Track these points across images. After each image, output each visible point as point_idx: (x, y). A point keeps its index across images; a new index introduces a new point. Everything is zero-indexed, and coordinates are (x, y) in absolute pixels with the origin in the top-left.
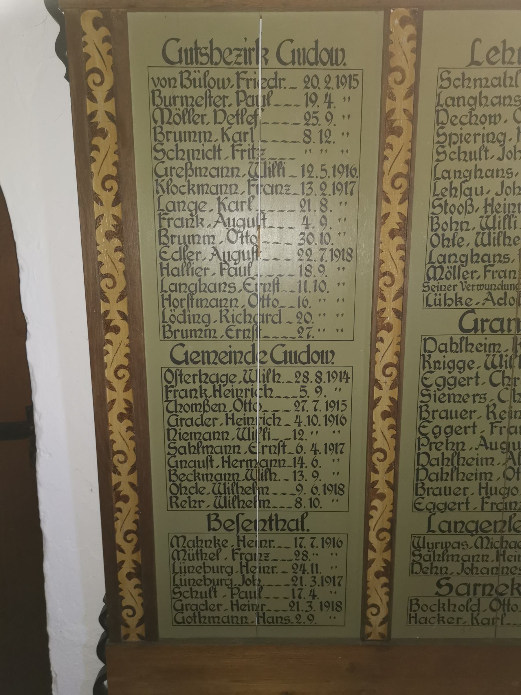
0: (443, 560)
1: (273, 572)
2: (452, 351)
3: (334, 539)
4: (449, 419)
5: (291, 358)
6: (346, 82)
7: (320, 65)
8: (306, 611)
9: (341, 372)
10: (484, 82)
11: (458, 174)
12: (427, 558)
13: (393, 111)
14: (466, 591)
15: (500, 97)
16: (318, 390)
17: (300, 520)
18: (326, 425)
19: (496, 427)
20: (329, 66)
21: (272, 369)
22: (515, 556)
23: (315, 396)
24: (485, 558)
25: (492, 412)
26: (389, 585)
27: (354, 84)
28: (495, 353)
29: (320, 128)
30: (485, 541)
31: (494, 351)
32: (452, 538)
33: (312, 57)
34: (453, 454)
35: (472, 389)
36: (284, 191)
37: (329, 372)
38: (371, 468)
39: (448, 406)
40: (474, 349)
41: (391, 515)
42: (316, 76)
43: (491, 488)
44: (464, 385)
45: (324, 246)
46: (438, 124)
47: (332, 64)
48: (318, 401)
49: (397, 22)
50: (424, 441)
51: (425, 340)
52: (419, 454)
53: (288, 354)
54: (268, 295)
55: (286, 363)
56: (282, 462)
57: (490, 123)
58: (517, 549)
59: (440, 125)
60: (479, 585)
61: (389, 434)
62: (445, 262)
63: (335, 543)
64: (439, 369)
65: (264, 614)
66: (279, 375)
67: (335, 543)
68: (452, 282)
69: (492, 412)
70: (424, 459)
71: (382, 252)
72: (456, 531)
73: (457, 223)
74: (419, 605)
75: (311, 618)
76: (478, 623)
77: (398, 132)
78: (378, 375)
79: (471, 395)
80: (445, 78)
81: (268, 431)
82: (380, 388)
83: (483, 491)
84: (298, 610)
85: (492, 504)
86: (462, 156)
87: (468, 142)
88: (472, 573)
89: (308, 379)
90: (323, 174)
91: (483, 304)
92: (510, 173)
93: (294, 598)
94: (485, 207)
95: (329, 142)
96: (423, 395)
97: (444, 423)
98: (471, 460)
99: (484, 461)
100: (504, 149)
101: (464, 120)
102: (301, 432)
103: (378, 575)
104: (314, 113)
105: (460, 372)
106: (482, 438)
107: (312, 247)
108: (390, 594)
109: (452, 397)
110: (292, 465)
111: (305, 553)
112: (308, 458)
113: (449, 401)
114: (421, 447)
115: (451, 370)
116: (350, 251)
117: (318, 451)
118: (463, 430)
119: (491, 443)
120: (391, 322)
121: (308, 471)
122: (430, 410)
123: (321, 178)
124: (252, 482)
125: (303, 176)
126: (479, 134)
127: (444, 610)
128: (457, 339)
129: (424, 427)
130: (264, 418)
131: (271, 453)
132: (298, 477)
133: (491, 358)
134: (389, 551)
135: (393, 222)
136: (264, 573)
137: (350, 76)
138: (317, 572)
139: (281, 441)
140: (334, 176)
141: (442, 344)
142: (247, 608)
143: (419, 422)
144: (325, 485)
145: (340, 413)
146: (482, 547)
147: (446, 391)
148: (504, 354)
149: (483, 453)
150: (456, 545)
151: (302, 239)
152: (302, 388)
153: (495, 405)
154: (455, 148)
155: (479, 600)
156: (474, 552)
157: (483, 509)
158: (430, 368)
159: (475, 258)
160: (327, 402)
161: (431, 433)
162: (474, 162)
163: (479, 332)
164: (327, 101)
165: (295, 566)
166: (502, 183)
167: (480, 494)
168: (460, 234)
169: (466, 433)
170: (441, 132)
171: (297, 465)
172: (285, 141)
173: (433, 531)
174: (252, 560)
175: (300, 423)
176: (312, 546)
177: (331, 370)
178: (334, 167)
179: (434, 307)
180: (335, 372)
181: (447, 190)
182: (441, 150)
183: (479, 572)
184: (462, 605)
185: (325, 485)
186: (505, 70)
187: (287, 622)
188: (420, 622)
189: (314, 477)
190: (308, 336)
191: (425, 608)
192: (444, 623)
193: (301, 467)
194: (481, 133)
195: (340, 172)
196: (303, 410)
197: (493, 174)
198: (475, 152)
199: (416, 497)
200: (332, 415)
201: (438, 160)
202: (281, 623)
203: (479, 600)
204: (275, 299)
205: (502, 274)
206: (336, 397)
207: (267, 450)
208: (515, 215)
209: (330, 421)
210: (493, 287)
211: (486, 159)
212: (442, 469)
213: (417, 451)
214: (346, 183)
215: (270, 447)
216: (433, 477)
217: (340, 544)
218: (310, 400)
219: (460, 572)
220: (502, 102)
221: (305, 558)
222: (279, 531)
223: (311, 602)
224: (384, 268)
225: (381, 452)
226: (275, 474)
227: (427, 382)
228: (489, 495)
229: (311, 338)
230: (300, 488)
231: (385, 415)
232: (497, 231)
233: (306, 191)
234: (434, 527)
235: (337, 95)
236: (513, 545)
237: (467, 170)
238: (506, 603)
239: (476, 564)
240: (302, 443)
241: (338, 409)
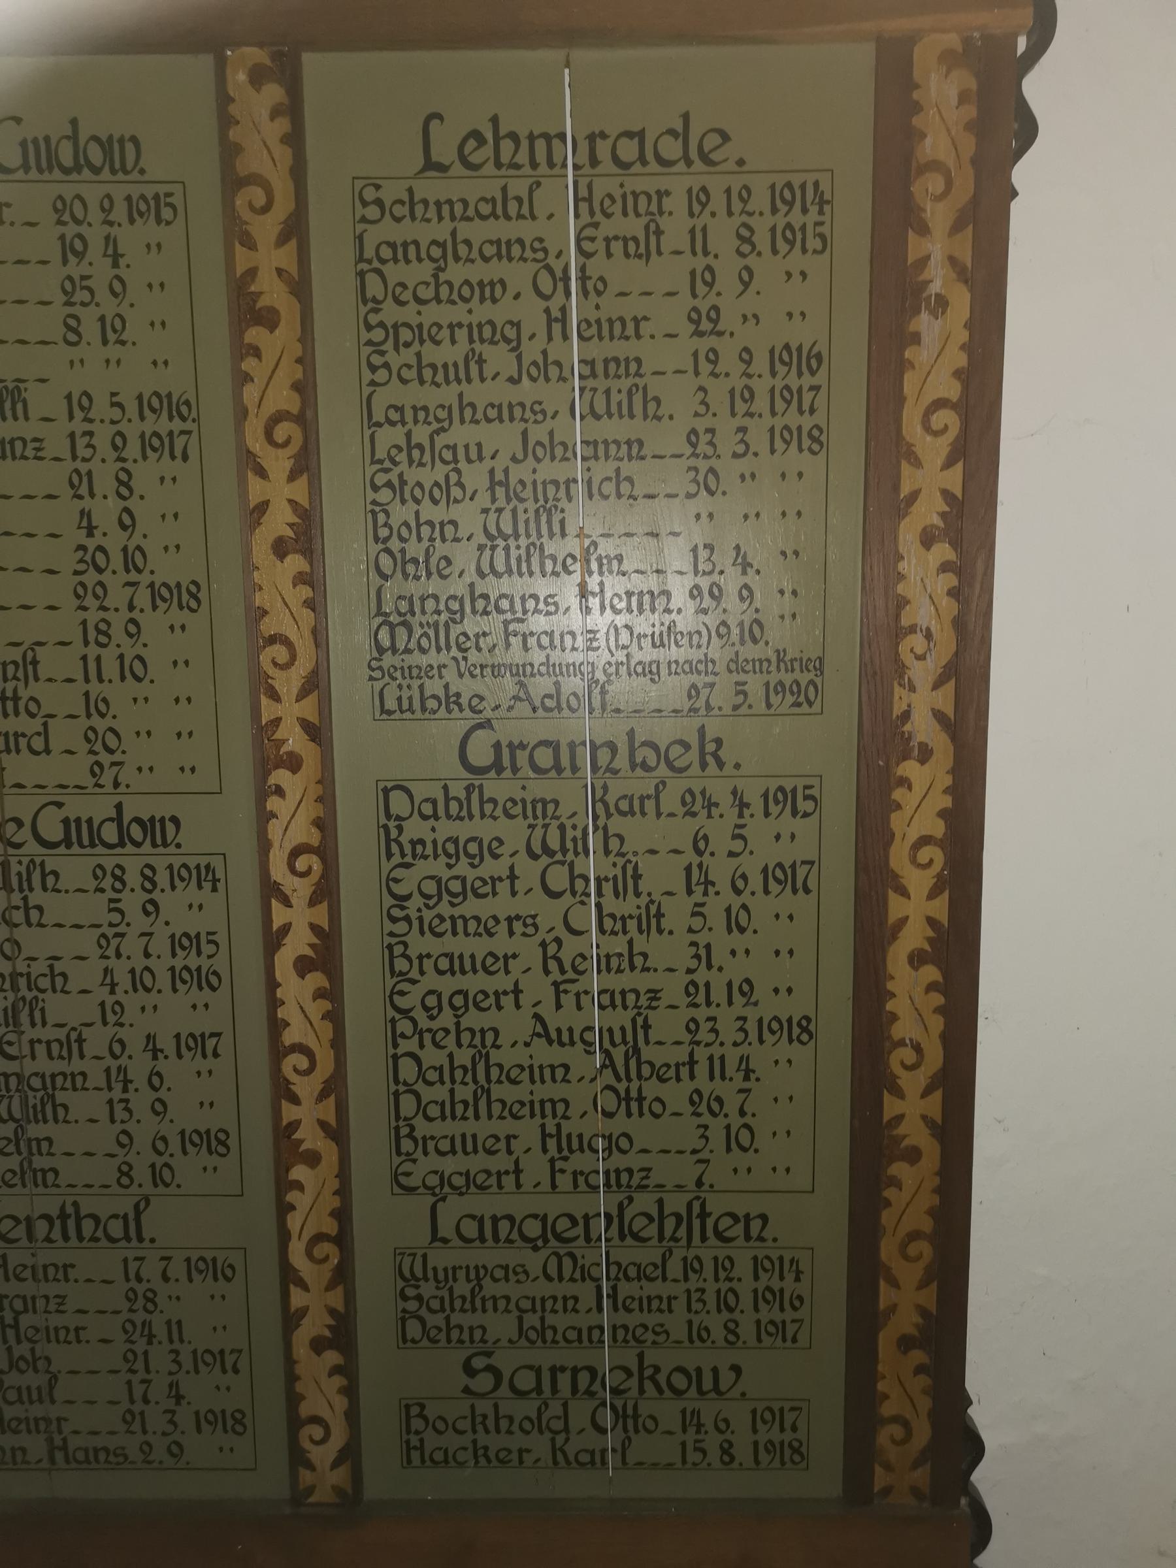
0: (474, 1310)
1: (79, 1341)
2: (449, 817)
3: (214, 1260)
4: (458, 974)
5: (77, 834)
6: (149, 210)
7: (86, 173)
8: (164, 1434)
9: (198, 867)
10: (459, 208)
11: (421, 415)
12: (435, 1304)
13: (252, 273)
14: (533, 1385)
15: (498, 242)
16: (150, 908)
17: (131, 1216)
18: (175, 990)
19: (566, 992)
20: (106, 174)
21: (38, 860)
22: (641, 1299)
23: (139, 922)
24: (570, 1304)
25: (555, 957)
26: (347, 1370)
27: (167, 213)
28: (547, 821)
29: (99, 312)
30: (567, 1263)
31: (545, 816)
32: (491, 1256)
33: (66, 155)
34: (474, 1057)
35: (502, 905)
36: (29, 453)
37: (170, 867)
38: (283, 1092)
39: (451, 944)
40: (499, 812)
41: (336, 1202)
42: (78, 197)
43: (569, 1136)
44: (485, 896)
45: (133, 576)
46: (365, 302)
47: (113, 171)
48: (151, 934)
49: (242, 77)
50: (404, 1026)
51: (386, 791)
52: (395, 1058)
53: (73, 825)
54: (15, 690)
55: (69, 846)
56: (79, 1079)
57: (482, 299)
58: (644, 1282)
59: (370, 305)
60: (563, 1369)
61: (316, 1009)
62: (413, 614)
63: (217, 1270)
64: (426, 857)
65: (65, 1440)
66: (55, 874)
67: (217, 1270)
68: (433, 658)
69: (555, 957)
70: (408, 1070)
71: (261, 589)
72: (496, 1239)
73: (430, 523)
74: (426, 1419)
75: (175, 1449)
76: (568, 1462)
77: (269, 319)
78: (278, 871)
79: (502, 917)
80: (369, 199)
81: (41, 1004)
82: (287, 903)
83: (552, 1144)
84: (145, 1432)
85: (575, 1174)
86: (427, 373)
87: (438, 343)
88: (544, 1341)
89: (124, 883)
90: (116, 413)
91: (510, 708)
92: (539, 411)
93: (132, 1401)
94: (492, 489)
95: (123, 343)
96: (394, 920)
97: (447, 984)
98: (518, 1070)
99: (547, 1073)
100: (519, 358)
101: (424, 293)
102: (117, 1008)
103: (318, 1345)
104: (83, 278)
105: (473, 866)
106: (536, 1016)
107: (106, 577)
108: (350, 1391)
109: (460, 922)
110: (104, 1084)
111: (150, 1295)
112: (139, 1067)
113: (455, 933)
114: (399, 1040)
115: (453, 861)
116: (193, 589)
117: (162, 1051)
118: (492, 999)
119: (559, 1031)
120: (297, 750)
121: (141, 1100)
122: (413, 953)
123: (113, 422)
124: (12, 1125)
125: (71, 417)
126: (460, 325)
127: (487, 1431)
128: (457, 790)
129: (402, 993)
130: (29, 974)
131: (51, 1057)
132: (120, 1114)
133: (539, 832)
134: (340, 1290)
135: (279, 521)
136: (58, 1341)
137: (156, 197)
138: (181, 1341)
139: (74, 1029)
140: (142, 417)
141: (426, 800)
142: (23, 1427)
143: (390, 982)
144: (182, 1133)
145: (205, 964)
146: (561, 1278)
147: (444, 909)
148: (568, 824)
149: (544, 1054)
150: (499, 1273)
151: (81, 561)
152: (112, 905)
153: (558, 941)
154: (408, 356)
155: (565, 1405)
156: (542, 1289)
157: (554, 1186)
158: (403, 855)
159: (480, 604)
160: (173, 936)
161: (419, 1007)
162: (455, 388)
163: (508, 773)
164: (110, 251)
165: (129, 1326)
166: (525, 433)
167: (545, 1150)
168: (440, 549)
169: (499, 1008)
170: (373, 319)
171: (113, 1085)
172: (22, 342)
173: (445, 1241)
174: (26, 1311)
175: (113, 986)
176: (165, 1278)
177: (177, 862)
178: (140, 398)
179: (397, 715)
180: (185, 866)
181: (400, 449)
182: (377, 360)
183: (559, 1337)
184: (528, 1418)
185: (182, 1133)
186: (503, 182)
187: (121, 1459)
188: (432, 1460)
189: (157, 1114)
190: (116, 784)
191: (440, 1426)
192: (489, 1461)
193: (125, 1090)
194: (466, 323)
195: (153, 410)
196: (118, 955)
197: (500, 413)
198: (455, 365)
199: (397, 1160)
200: (186, 968)
201: (373, 383)
202: (106, 1461)
203: (565, 1405)
204: (32, 699)
205: (545, 640)
206: (194, 924)
207: (41, 1050)
208: (560, 505)
209: (184, 982)
210: (528, 669)
211: (483, 380)
212: (452, 1091)
213: (391, 1051)
214: (171, 434)
215: (48, 1043)
216: (433, 1111)
217: (229, 1272)
218: (132, 932)
219: (515, 1338)
220: (504, 252)
221: (150, 1306)
222: (85, 1244)
223: (173, 1412)
224: (269, 626)
225: (301, 1052)
226: (66, 1107)
227: (399, 889)
228: (565, 1153)
229: (122, 789)
230: (125, 1139)
231: (303, 966)
232: (523, 542)
233: (82, 452)
234: (446, 1229)
235: (131, 238)
236: (632, 1272)
237: (443, 407)
238: (630, 1412)
239: (551, 1319)
240: (123, 1033)
241: (199, 953)
